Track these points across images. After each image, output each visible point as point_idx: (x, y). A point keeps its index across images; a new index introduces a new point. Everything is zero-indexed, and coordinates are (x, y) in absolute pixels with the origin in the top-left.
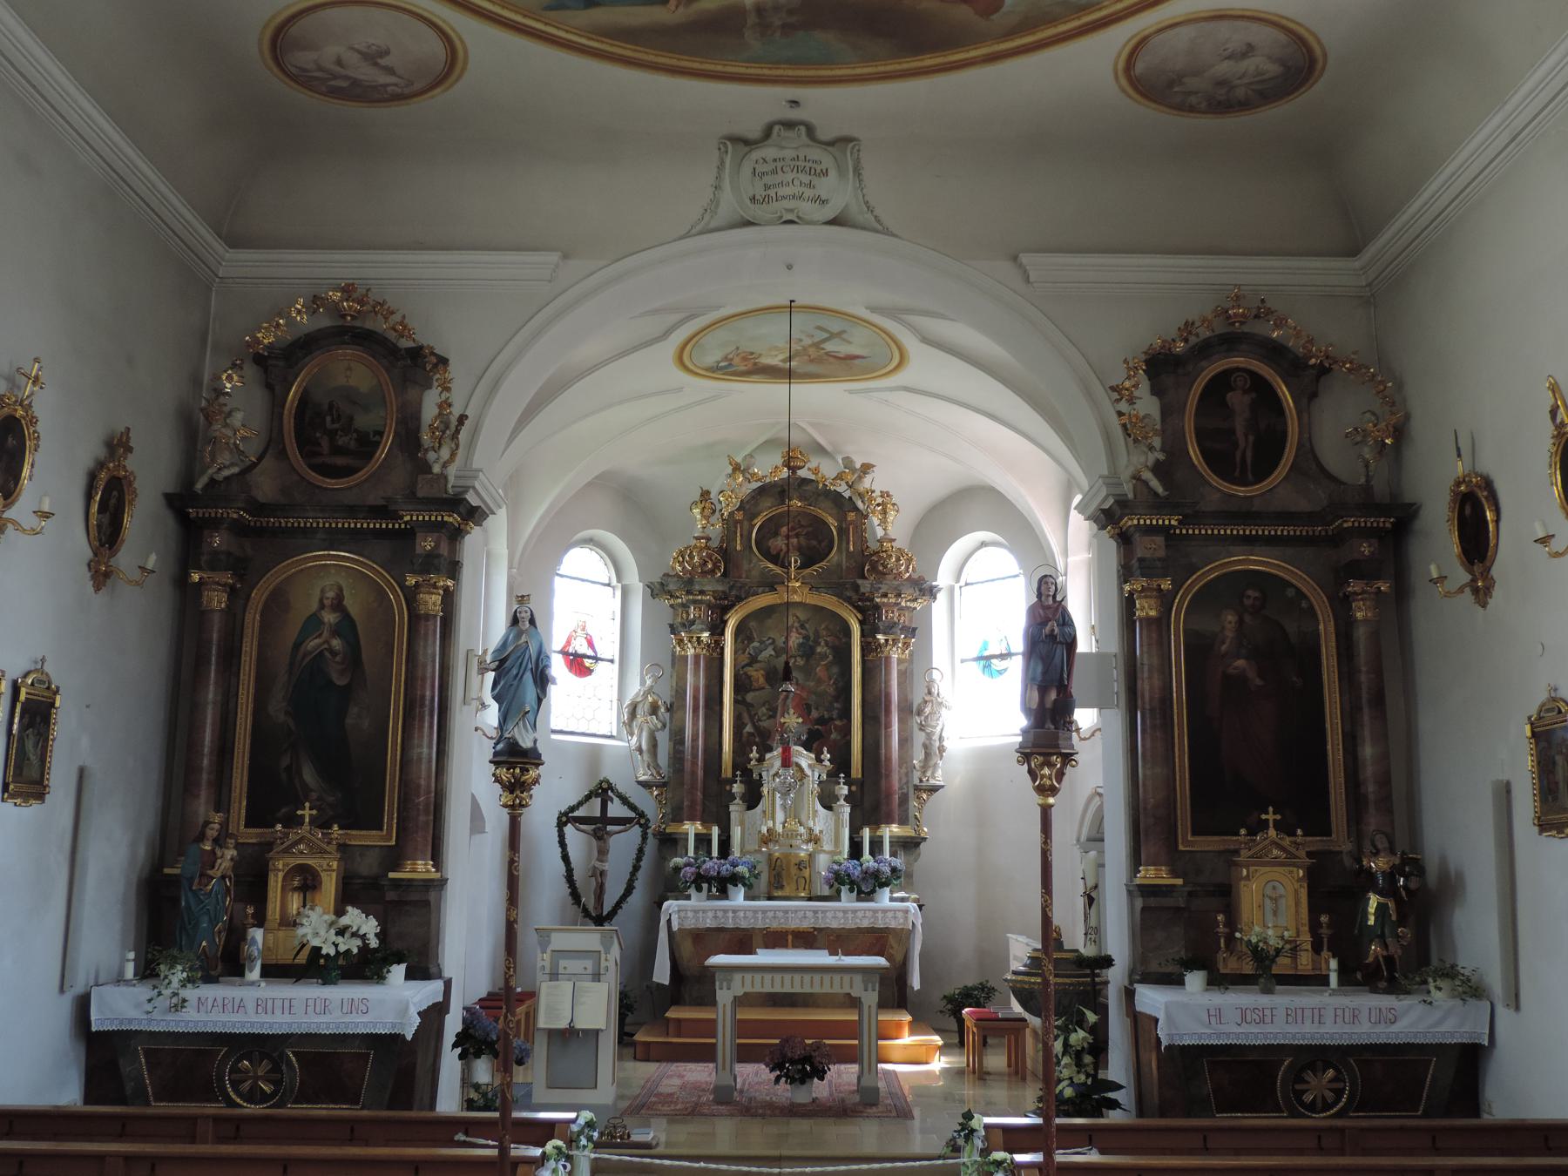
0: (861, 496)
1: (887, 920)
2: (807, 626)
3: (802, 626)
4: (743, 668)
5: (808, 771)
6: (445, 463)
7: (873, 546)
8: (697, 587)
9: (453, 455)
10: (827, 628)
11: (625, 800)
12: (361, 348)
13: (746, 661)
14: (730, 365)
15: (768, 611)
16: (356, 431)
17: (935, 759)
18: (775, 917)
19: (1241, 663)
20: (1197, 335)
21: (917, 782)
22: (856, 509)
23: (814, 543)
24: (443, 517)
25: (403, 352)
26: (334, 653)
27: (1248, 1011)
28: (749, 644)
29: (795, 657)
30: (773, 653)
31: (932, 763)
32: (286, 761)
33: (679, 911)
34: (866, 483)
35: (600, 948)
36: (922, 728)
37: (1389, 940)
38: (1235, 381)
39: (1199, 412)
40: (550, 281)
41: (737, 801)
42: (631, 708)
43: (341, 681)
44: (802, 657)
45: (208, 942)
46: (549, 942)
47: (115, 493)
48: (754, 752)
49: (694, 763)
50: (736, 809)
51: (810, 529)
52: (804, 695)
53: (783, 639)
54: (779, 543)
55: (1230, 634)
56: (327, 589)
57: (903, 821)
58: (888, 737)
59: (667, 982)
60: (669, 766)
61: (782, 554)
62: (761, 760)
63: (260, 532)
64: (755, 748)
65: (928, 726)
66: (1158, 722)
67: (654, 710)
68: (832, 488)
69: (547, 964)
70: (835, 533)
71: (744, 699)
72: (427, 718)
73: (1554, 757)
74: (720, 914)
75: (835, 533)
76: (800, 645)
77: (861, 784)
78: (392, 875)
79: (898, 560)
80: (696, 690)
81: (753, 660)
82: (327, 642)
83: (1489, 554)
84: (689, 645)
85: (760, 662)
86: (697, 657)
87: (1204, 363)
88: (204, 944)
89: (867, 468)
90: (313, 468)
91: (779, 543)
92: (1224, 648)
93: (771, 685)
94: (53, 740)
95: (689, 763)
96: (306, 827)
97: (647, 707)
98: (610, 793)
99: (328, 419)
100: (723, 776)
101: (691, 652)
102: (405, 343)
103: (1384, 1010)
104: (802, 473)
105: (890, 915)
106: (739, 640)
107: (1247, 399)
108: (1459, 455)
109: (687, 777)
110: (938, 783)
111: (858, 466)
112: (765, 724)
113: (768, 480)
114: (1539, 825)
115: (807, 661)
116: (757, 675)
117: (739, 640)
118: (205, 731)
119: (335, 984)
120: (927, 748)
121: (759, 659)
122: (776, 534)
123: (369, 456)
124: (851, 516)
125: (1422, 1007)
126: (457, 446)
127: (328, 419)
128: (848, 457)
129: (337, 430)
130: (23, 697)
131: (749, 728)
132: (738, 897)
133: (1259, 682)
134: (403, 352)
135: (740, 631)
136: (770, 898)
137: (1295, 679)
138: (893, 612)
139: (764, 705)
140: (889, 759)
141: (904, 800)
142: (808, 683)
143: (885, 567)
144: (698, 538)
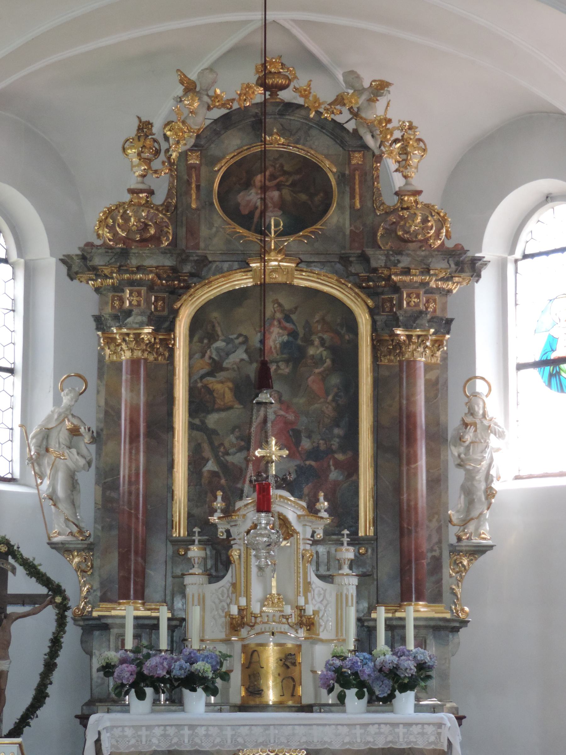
2: (294, 317)
3: (287, 318)
4: (202, 377)
10: (323, 320)
13: (206, 369)
22: (365, 147)
23: (303, 197)
30: (245, 356)
31: (475, 513)
44: (287, 361)
48: (219, 499)
51: (297, 177)
52: (291, 417)
64: (220, 494)
71: (203, 422)
76: (284, 345)
79: (425, 220)
84: (124, 346)
85: (227, 369)
93: (241, 403)
97: (64, 436)
117: (196, 339)
121: (225, 365)
122: (247, 185)
124: (357, 158)
128: (352, 72)
131: (211, 466)
138: (418, 296)
142: (295, 400)
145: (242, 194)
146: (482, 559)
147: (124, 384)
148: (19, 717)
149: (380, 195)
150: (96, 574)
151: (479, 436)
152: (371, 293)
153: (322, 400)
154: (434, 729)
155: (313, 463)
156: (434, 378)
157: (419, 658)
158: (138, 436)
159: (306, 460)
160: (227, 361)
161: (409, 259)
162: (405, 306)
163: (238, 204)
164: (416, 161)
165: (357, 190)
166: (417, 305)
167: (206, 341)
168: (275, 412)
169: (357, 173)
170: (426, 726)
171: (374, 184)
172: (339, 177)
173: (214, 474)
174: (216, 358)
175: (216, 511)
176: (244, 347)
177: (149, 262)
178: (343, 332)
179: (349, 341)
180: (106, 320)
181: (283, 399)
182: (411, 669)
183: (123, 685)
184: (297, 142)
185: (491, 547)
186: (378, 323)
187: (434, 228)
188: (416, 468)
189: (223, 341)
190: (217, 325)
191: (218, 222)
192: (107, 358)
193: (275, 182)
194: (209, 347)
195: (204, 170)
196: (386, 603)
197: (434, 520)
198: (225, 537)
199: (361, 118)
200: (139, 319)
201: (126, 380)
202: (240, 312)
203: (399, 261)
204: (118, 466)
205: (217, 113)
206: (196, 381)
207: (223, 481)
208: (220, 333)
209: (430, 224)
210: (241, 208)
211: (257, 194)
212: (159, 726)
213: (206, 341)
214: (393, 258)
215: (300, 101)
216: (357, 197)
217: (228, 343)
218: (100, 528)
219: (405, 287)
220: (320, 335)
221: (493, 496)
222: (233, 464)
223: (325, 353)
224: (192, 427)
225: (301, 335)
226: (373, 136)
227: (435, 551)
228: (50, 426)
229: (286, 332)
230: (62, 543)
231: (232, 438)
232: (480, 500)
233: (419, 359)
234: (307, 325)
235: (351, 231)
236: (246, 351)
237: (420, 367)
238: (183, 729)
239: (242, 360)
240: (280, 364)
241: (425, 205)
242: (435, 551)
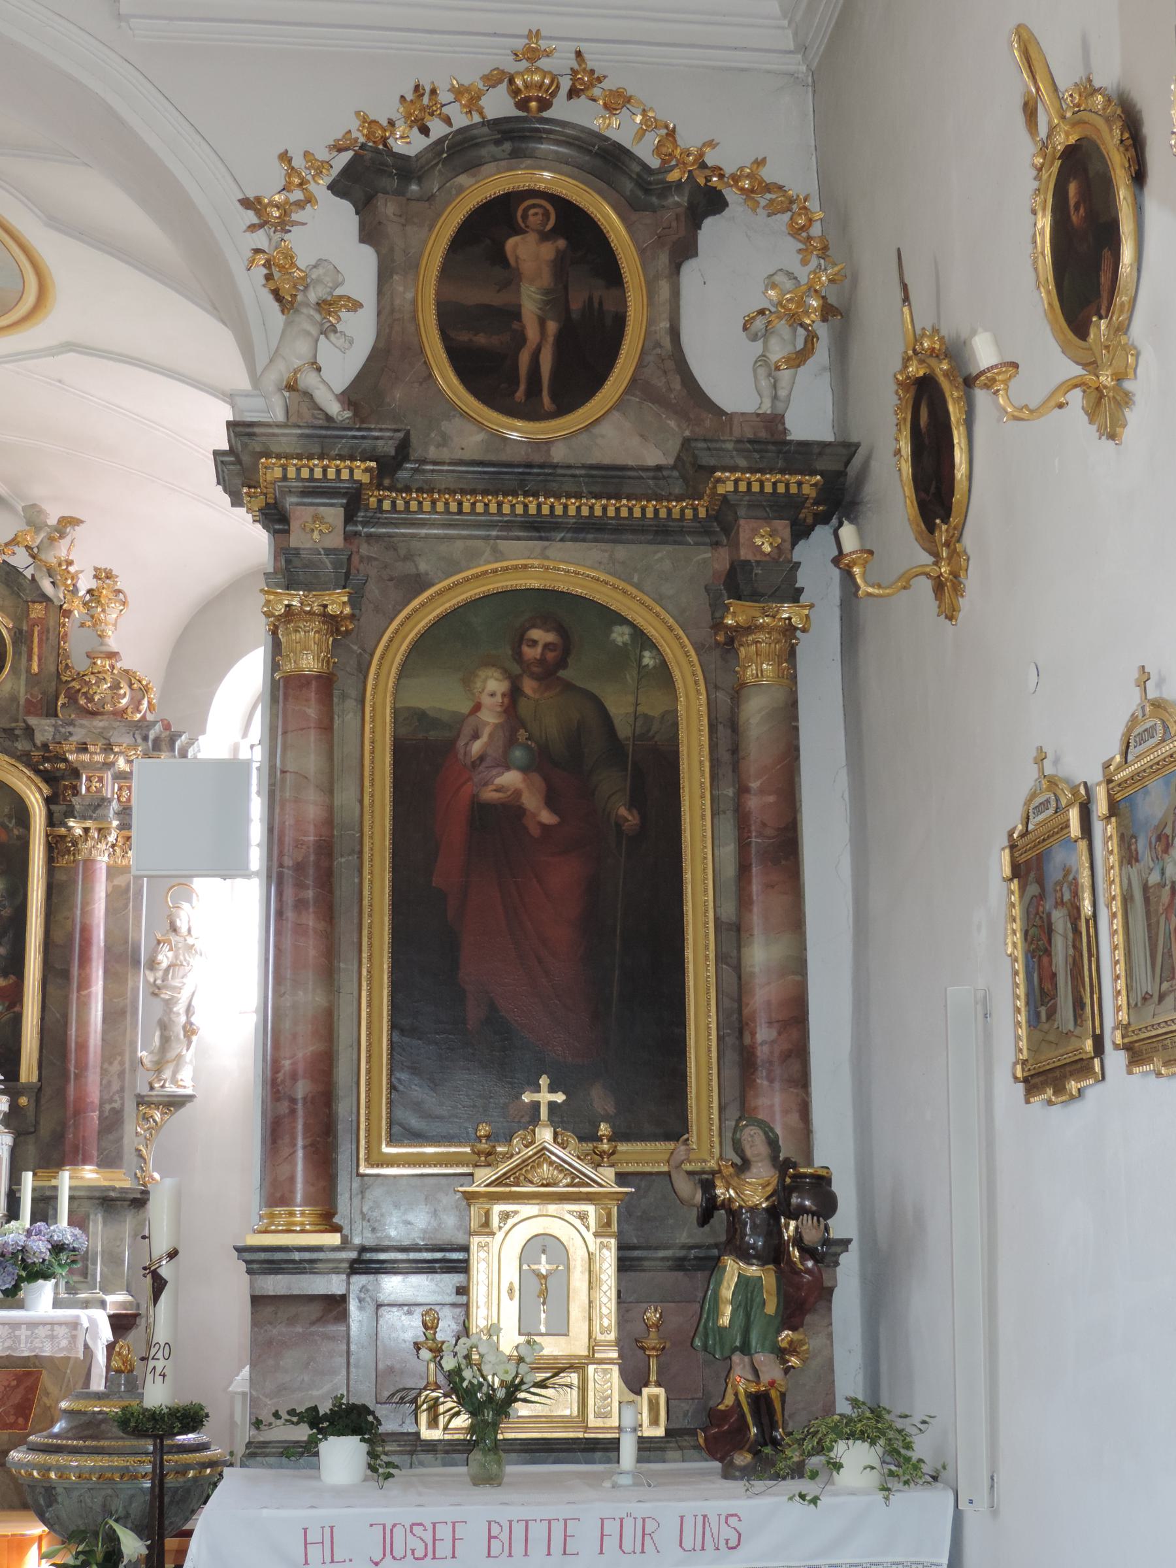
0: (50, 572)
1: (37, 1344)
7: (79, 663)
17: (177, 1048)
19: (511, 778)
20: (448, 121)
21: (145, 1091)
22: (45, 598)
27: (398, 1531)
31: (171, 1055)
34: (62, 550)
36: (155, 991)
37: (760, 1358)
38: (525, 217)
39: (447, 272)
55: (490, 717)
57: (108, 1161)
58: (84, 1005)
65: (166, 987)
66: (310, 894)
70: (8, 640)
73: (1049, 915)
75: (8, 640)
77: (37, 1092)
79: (116, 686)
83: (957, 496)
87: (463, 179)
89: (68, 523)
92: (476, 747)
103: (713, 1520)
105: (42, 1332)
107: (548, 251)
108: (906, 299)
110: (181, 1091)
111: (52, 521)
114: (1026, 1080)
120: (165, 1026)
124: (37, 611)
125: (798, 1506)
128: (34, 506)
133: (547, 817)
137: (623, 811)
138: (101, 780)
140: (82, 1047)
141: (112, 1122)
143: (90, 699)
146: (183, 1111)
149: (68, 657)
151: (181, 958)
152: (49, 778)
154: (67, 1330)
156: (123, 884)
157: (55, 1238)
161: (83, 731)
162: (83, 791)
164: (114, 616)
165: (36, 650)
166: (99, 790)
169: (36, 629)
170: (56, 1327)
171: (59, 643)
172: (15, 633)
178: (11, 826)
179: (19, 838)
182: (41, 1252)
185: (190, 1098)
186: (55, 815)
187: (127, 697)
188: (89, 995)
196: (594, 1200)
197: (116, 1063)
199: (40, 560)
203: (71, 734)
209: (122, 692)
214: (63, 730)
216: (35, 658)
219: (84, 768)
221: (194, 1032)
226: (53, 583)
227: (116, 1101)
232: (177, 1036)
233: (99, 858)
235: (27, 700)
237: (101, 868)
238: (20, 1329)
241: (124, 671)
242: (116, 1101)
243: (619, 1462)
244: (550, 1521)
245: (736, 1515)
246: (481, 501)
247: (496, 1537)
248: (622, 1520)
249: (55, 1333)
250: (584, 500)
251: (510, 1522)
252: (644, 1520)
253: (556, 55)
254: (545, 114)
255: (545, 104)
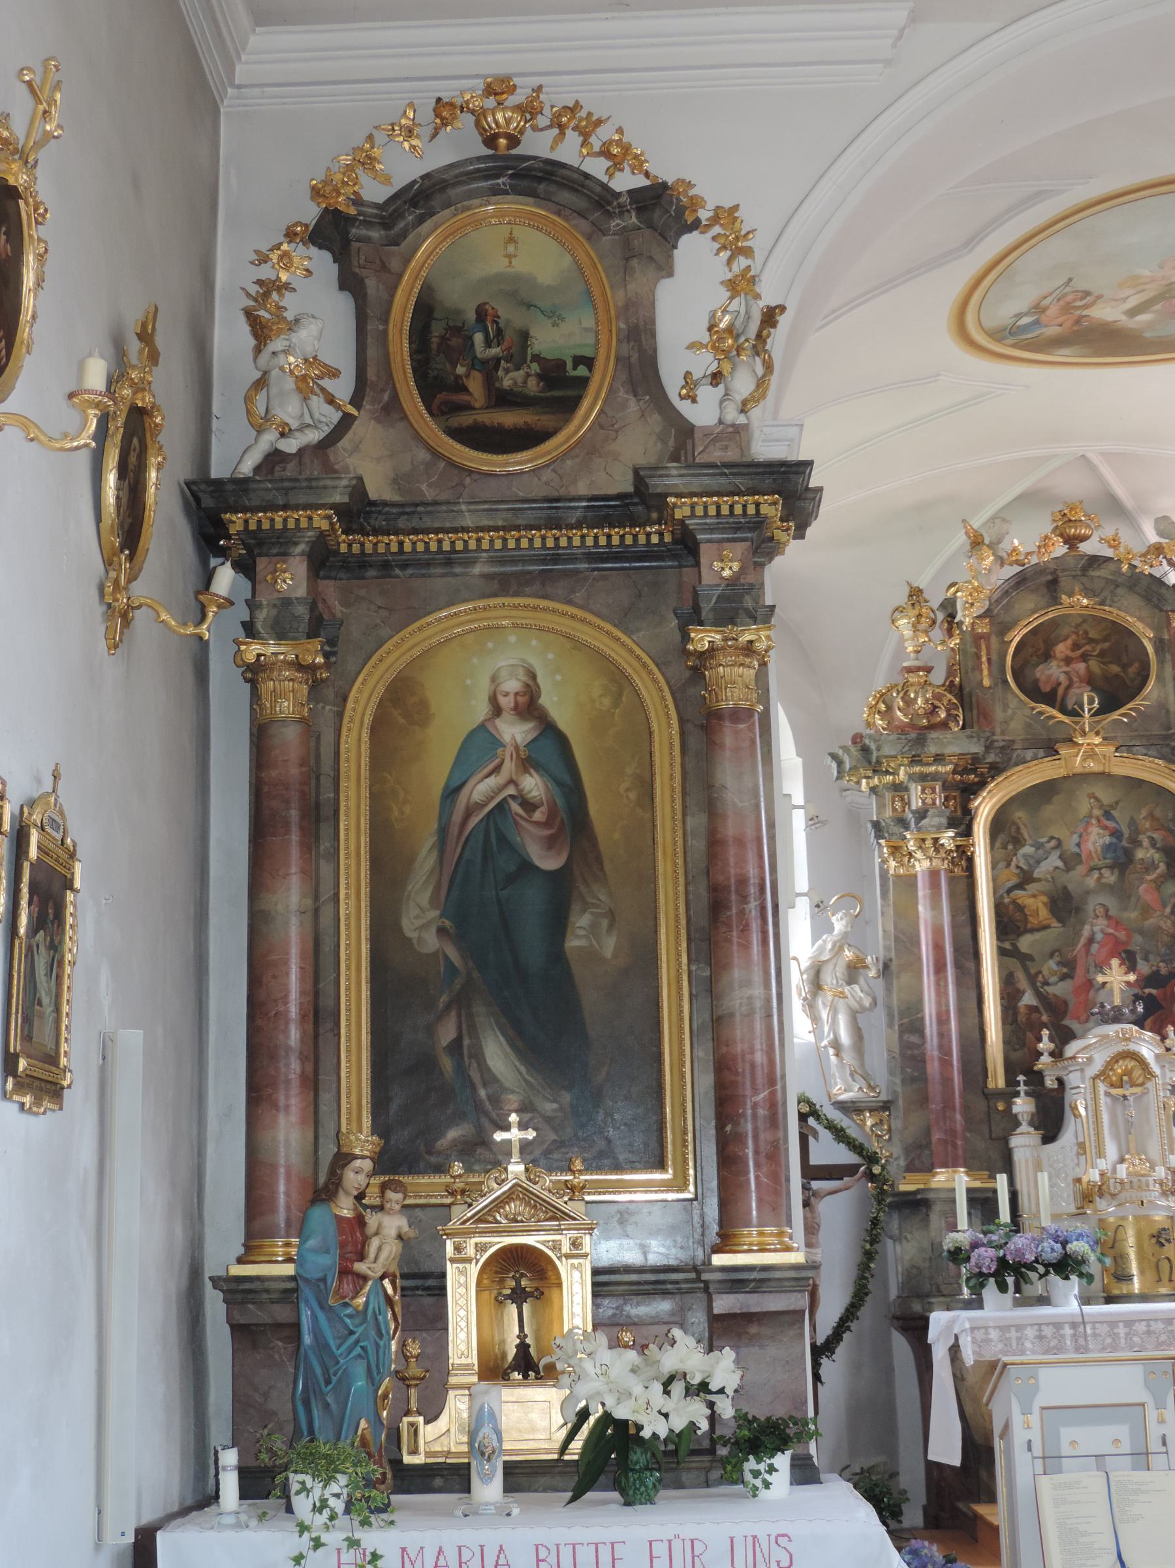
2: (1115, 813)
3: (1107, 815)
4: (1009, 891)
5: (1155, 1067)
6: (745, 403)
8: (932, 749)
9: (761, 384)
10: (1151, 815)
11: (839, 1134)
12: (530, 200)
13: (1014, 881)
14: (1036, 323)
15: (1045, 792)
16: (536, 358)
18: (1149, 1333)
23: (1115, 669)
24: (758, 505)
25: (624, 199)
26: (529, 806)
28: (1016, 850)
29: (1100, 869)
30: (1060, 864)
32: (447, 1033)
33: (973, 1329)
35: (1142, 1395)
40: (888, 62)
41: (1024, 1127)
42: (812, 973)
43: (549, 862)
44: (1111, 867)
45: (368, 1421)
46: (1036, 1389)
47: (135, 441)
48: (1045, 1039)
49: (946, 1063)
50: (1024, 1143)
51: (1106, 645)
52: (1122, 935)
53: (1075, 838)
54: (1052, 672)
56: (504, 674)
59: (957, 1462)
60: (891, 1073)
61: (1061, 691)
62: (1057, 1054)
63: (358, 566)
64: (1045, 1033)
67: (854, 971)
68: (1147, 570)
69: (1035, 1436)
70: (1150, 649)
71: (1014, 945)
72: (755, 926)
74: (1048, 1331)
75: (1150, 649)
76: (1107, 848)
78: (719, 1260)
80: (937, 932)
81: (1026, 879)
82: (511, 781)
84: (919, 855)
85: (1039, 880)
86: (934, 874)
88: (363, 1424)
90: (458, 434)
91: (1052, 672)
93: (1059, 920)
94: (73, 964)
95: (936, 1063)
96: (516, 1168)
97: (840, 971)
98: (811, 1121)
99: (478, 338)
100: (991, 1085)
101: (921, 865)
102: (625, 182)
104: (1088, 548)
106: (998, 844)
109: (935, 1089)
112: (1059, 989)
113: (1034, 560)
115: (1122, 874)
116: (1034, 902)
117: (998, 844)
118: (287, 974)
119: (650, 1501)
121: (1036, 875)
122: (1047, 656)
123: (568, 406)
126: (769, 367)
127: (478, 338)
128: (1166, 518)
129: (498, 360)
130: (33, 853)
131: (1028, 999)
132: (528, 1341)
134: (624, 199)
135: (998, 825)
136: (1110, 1300)
139: (1051, 955)
142: (1126, 915)
144: (909, 670)
145: (1040, 667)
147: (921, 901)
148: (837, 1320)
150: (896, 1139)
153: (1158, 913)
155: (1154, 992)
158: (945, 965)
159: (1145, 987)
160: (1037, 870)
163: (1037, 681)
167: (1010, 847)
168: (1102, 931)
173: (1032, 1009)
174: (1025, 867)
175: (1042, 1054)
176: (1058, 853)
177: (949, 750)
180: (888, 825)
181: (1110, 913)
183: (981, 1274)
184: (1102, 603)
189: (1032, 846)
190: (1022, 827)
191: (1013, 703)
192: (892, 872)
193: (1079, 652)
194: (1015, 854)
195: (994, 640)
198: (1056, 1086)
200: (936, 821)
201: (925, 897)
202: (1048, 811)
204: (920, 1001)
205: (1011, 571)
206: (1002, 897)
207: (1045, 1018)
208: (1026, 836)
210: (1041, 685)
211: (1059, 667)
212: (1032, 1325)
213: (1010, 847)
215: (1109, 553)
217: (1038, 849)
218: (898, 1081)
220: (1149, 834)
222: (1055, 995)
223: (1157, 856)
224: (1002, 952)
225: (1126, 835)
228: (823, 958)
229: (1107, 833)
230: (853, 1102)
231: (1052, 964)
234: (1133, 823)
236: (1061, 857)
238: (1118, 1327)
239: (1057, 868)
240: (1103, 871)
243: (469, 1492)
244: (574, 1545)
245: (785, 1535)
246: (525, 537)
247: (543, 1560)
248: (670, 1541)
249: (1097, 1331)
250: (628, 529)
251: (558, 1546)
252: (692, 1541)
253: (518, 90)
254: (514, 152)
255: (514, 141)
